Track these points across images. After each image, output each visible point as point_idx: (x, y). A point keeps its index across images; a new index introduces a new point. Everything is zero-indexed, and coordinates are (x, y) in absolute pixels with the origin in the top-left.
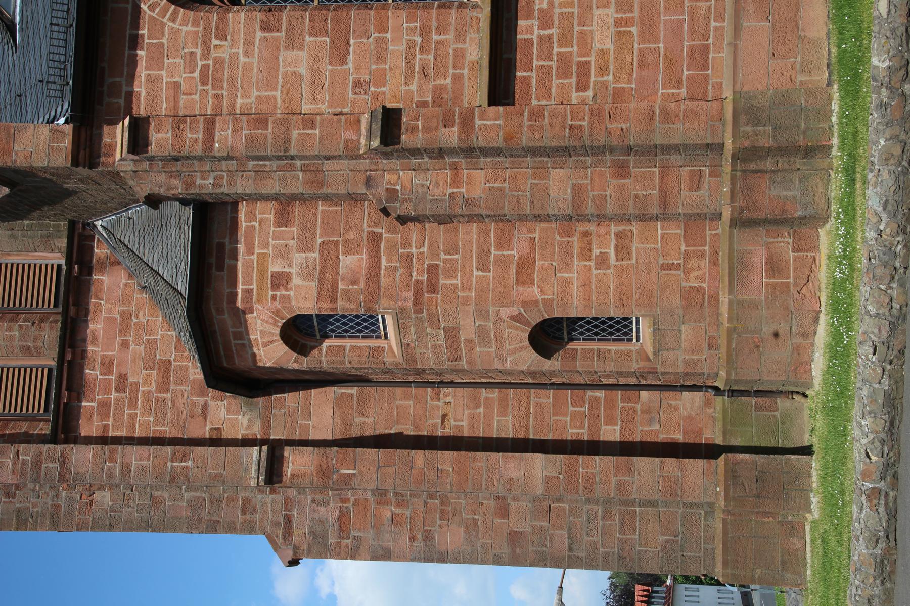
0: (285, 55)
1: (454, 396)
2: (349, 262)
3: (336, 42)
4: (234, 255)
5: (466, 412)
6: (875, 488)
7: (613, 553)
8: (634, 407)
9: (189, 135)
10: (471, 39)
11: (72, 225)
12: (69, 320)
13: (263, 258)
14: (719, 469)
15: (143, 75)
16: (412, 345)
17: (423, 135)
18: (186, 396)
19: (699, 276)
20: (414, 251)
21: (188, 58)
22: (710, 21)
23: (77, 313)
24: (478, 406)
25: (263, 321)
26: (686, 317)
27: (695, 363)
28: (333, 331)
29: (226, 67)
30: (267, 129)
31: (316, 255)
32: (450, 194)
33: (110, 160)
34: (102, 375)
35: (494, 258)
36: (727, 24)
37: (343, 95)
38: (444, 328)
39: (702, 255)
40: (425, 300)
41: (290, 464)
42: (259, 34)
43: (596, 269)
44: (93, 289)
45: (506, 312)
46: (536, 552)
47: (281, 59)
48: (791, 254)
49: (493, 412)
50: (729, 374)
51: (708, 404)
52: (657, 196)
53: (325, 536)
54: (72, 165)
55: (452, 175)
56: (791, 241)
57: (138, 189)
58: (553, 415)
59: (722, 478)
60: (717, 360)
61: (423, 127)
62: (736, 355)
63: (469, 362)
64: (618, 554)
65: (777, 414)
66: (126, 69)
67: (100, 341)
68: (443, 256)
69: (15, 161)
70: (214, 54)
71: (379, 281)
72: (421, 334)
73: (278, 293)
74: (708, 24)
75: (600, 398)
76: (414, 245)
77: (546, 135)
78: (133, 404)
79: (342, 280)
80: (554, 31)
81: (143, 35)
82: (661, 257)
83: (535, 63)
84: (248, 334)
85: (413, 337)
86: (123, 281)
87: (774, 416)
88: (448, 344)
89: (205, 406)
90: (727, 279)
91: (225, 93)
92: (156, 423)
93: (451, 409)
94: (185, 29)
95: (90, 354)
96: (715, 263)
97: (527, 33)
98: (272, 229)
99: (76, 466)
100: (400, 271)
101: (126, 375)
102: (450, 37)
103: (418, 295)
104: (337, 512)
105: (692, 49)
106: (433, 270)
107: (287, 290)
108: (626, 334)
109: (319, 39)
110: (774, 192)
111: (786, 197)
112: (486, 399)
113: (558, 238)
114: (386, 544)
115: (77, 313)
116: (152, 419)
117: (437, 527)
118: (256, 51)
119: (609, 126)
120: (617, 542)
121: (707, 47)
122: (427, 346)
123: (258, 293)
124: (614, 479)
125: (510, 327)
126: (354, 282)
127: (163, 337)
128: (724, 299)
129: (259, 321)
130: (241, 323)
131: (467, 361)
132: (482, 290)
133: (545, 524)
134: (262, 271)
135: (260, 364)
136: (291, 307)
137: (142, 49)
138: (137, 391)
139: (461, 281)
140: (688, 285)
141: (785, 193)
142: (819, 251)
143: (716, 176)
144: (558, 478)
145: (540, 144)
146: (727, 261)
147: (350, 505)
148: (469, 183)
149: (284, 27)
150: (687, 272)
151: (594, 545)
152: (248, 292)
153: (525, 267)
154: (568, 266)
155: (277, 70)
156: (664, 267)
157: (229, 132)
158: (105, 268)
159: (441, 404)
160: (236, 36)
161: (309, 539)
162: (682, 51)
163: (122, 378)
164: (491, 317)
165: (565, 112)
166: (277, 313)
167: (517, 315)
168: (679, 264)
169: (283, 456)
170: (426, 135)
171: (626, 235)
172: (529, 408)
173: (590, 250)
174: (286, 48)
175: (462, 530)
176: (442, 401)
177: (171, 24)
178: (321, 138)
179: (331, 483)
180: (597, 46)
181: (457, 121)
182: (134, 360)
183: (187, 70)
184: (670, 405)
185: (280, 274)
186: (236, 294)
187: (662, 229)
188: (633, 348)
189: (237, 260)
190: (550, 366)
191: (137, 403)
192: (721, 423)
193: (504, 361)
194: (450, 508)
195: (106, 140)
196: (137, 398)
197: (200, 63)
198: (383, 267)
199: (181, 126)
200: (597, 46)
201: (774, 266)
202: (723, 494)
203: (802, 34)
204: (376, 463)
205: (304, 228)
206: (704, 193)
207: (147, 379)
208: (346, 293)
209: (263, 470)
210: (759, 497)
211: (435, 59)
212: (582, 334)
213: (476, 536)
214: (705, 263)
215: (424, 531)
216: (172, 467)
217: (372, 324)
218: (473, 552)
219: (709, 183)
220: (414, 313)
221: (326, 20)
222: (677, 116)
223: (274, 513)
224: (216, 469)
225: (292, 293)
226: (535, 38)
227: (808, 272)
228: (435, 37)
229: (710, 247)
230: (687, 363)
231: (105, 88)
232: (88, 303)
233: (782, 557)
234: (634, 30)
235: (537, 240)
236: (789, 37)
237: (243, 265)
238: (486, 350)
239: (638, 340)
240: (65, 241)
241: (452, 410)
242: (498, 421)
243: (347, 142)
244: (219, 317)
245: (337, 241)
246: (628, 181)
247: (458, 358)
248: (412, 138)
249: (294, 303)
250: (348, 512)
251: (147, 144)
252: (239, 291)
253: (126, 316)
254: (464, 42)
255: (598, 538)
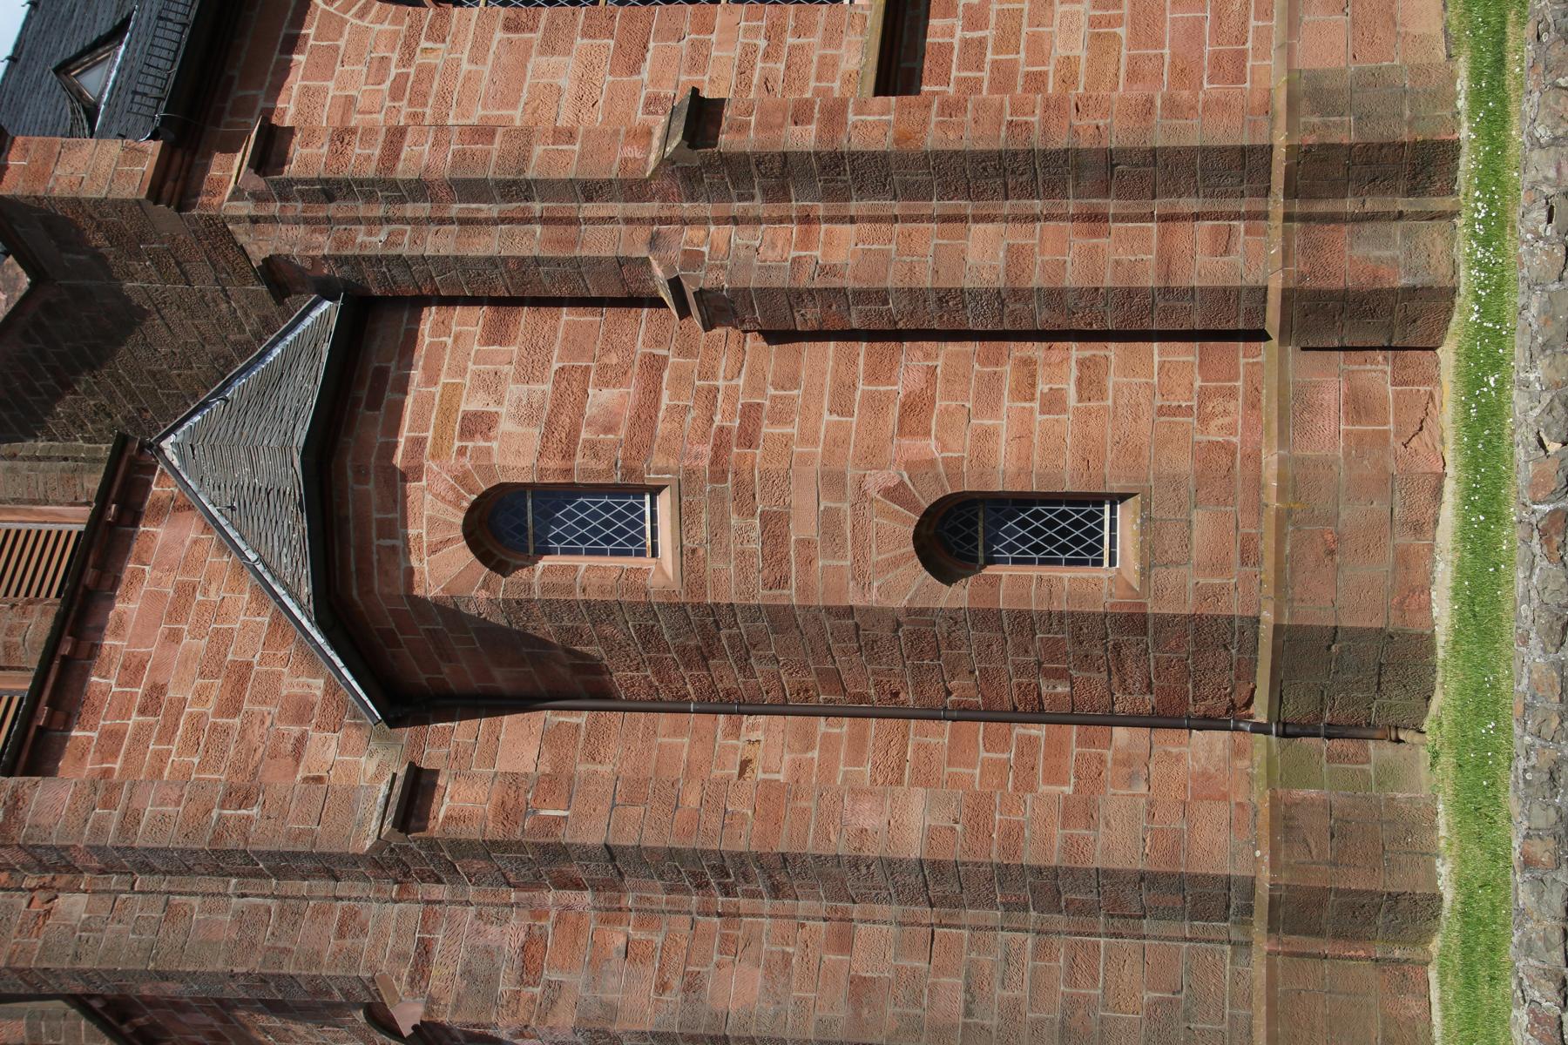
0: (536, 61)
1: (767, 730)
2: (601, 398)
3: (625, 45)
4: (403, 386)
5: (786, 757)
6: (1556, 511)
7: (1052, 1021)
8: (1101, 755)
9: (358, 151)
10: (849, 42)
11: (122, 443)
12: (81, 590)
13: (452, 392)
14: (1260, 817)
15: (295, 87)
16: (701, 552)
17: (757, 133)
18: (268, 723)
19: (1227, 424)
20: (721, 383)
21: (375, 64)
22: (1247, 20)
23: (98, 581)
24: (809, 747)
25: (436, 496)
26: (1202, 493)
27: (1217, 593)
28: (558, 538)
29: (437, 77)
30: (492, 143)
31: (548, 387)
32: (794, 259)
33: (216, 201)
34: (119, 685)
35: (862, 396)
36: (1276, 23)
37: (628, 114)
38: (762, 512)
39: (1232, 394)
40: (732, 458)
41: (447, 799)
42: (499, 35)
43: (1042, 412)
44: (135, 547)
45: (876, 480)
46: (902, 1017)
47: (530, 67)
48: (1390, 389)
49: (838, 759)
50: (1278, 613)
51: (1238, 752)
52: (1154, 262)
53: (491, 980)
54: (149, 197)
55: (800, 231)
56: (1389, 369)
57: (255, 248)
58: (949, 764)
59: (1265, 832)
60: (1256, 588)
61: (758, 124)
62: (1293, 571)
63: (803, 590)
64: (1062, 1022)
65: (1370, 768)
66: (269, 79)
67: (130, 630)
68: (771, 391)
69: (52, 189)
70: (419, 59)
71: (653, 428)
72: (719, 527)
73: (470, 444)
74: (1245, 23)
75: (1037, 738)
76: (722, 374)
77: (967, 134)
78: (167, 735)
79: (588, 425)
80: (989, 33)
81: (306, 36)
82: (1158, 396)
83: (954, 73)
84: (405, 526)
85: (704, 533)
86: (193, 535)
87: (1363, 771)
88: (767, 551)
89: (301, 741)
90: (1275, 425)
91: (428, 111)
92: (202, 767)
93: (758, 753)
94: (377, 27)
95: (105, 651)
96: (1253, 405)
97: (943, 35)
98: (476, 347)
99: (35, 814)
100: (693, 413)
101: (163, 686)
102: (816, 39)
103: (720, 449)
104: (522, 935)
105: (1217, 59)
106: (751, 413)
107: (488, 439)
108: (1091, 549)
109: (598, 42)
110: (1359, 252)
111: (1378, 258)
112: (826, 736)
113: (977, 366)
114: (609, 997)
115: (98, 581)
116: (196, 760)
117: (712, 967)
118: (491, 57)
119: (1076, 122)
120: (1059, 999)
121: (1243, 53)
122: (727, 554)
123: (435, 445)
124: (1058, 833)
125: (882, 513)
126: (609, 429)
127: (245, 625)
128: (1270, 461)
129: (429, 497)
130: (395, 501)
131: (798, 588)
132: (836, 443)
133: (923, 965)
134: (446, 413)
135: (418, 592)
136: (490, 468)
137: (302, 52)
138: (180, 714)
139: (801, 429)
140: (1204, 438)
141: (1377, 253)
142: (1439, 382)
143: (1258, 234)
144: (953, 829)
145: (956, 147)
146: (1275, 399)
147: (548, 924)
148: (829, 244)
149: (542, 26)
150: (1204, 420)
151: (1014, 1007)
152: (418, 443)
153: (915, 412)
154: (993, 408)
155: (521, 81)
156: (1161, 411)
157: (427, 148)
158: (164, 515)
159: (740, 744)
160: (461, 37)
161: (460, 984)
162: (1201, 57)
163: (157, 690)
164: (849, 491)
165: (1002, 104)
166: (463, 479)
167: (895, 488)
168: (1191, 408)
169: (435, 784)
170: (762, 136)
171: (1096, 364)
172: (905, 753)
173: (1033, 385)
174: (541, 53)
175: (760, 972)
176: (743, 739)
177: (356, 21)
178: (582, 156)
179: (519, 832)
180: (1059, 51)
181: (817, 115)
182: (184, 663)
183: (370, 81)
184: (1168, 754)
185: (478, 415)
186: (395, 445)
187: (1161, 354)
188: (1102, 575)
189: (406, 393)
190: (950, 599)
191: (174, 733)
192: (1263, 783)
193: (865, 587)
194: (740, 933)
195: (214, 172)
196: (177, 725)
197: (393, 72)
198: (663, 407)
199: (347, 138)
200: (1059, 51)
201: (1359, 405)
202: (1267, 858)
203: (1402, 30)
204: (609, 800)
205: (532, 347)
206: (1236, 258)
207: (200, 696)
208: (592, 446)
209: (392, 809)
210: (1335, 865)
211: (788, 67)
212: (1011, 548)
213: (787, 985)
214: (1237, 406)
215: (686, 973)
216: (220, 817)
217: (632, 524)
218: (776, 1015)
219: (1246, 244)
220: (711, 481)
221: (612, 17)
222: (1193, 108)
223: (400, 936)
224: (304, 821)
225: (495, 445)
226: (956, 43)
227: (1421, 415)
228: (790, 40)
229: (1245, 382)
230: (1203, 594)
231: (229, 105)
232: (121, 570)
233: (1384, 1031)
234: (1122, 31)
235: (939, 370)
236: (1379, 34)
237: (415, 400)
238: (835, 563)
239: (1112, 563)
240: (100, 476)
241: (760, 754)
242: (846, 773)
243: (625, 161)
244: (356, 487)
245: (588, 368)
246: (1104, 240)
247: (781, 582)
248: (738, 138)
249: (495, 460)
250: (543, 937)
251: (283, 160)
252: (402, 441)
253: (186, 591)
254: (839, 46)
255: (1023, 993)
